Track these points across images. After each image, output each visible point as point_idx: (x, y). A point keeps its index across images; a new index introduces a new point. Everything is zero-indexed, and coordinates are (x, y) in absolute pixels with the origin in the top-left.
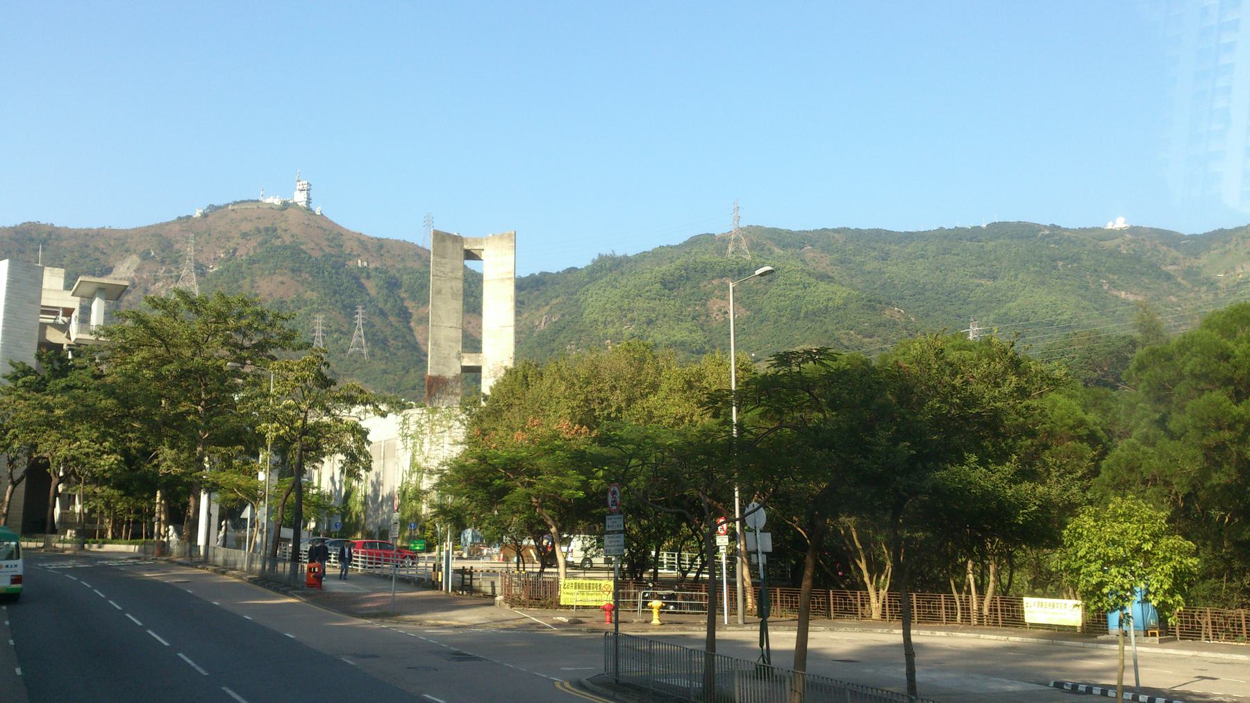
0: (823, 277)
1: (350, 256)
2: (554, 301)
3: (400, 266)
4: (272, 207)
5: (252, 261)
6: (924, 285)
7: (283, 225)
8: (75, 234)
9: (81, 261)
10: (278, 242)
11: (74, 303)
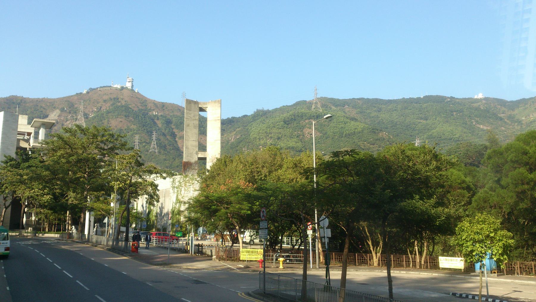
0: (353, 119)
1: (150, 110)
2: (238, 130)
3: (172, 114)
4: (116, 89)
5: (108, 112)
6: (396, 122)
7: (121, 97)
8: (32, 101)
9: (35, 112)
10: (119, 104)
11: (32, 130)
